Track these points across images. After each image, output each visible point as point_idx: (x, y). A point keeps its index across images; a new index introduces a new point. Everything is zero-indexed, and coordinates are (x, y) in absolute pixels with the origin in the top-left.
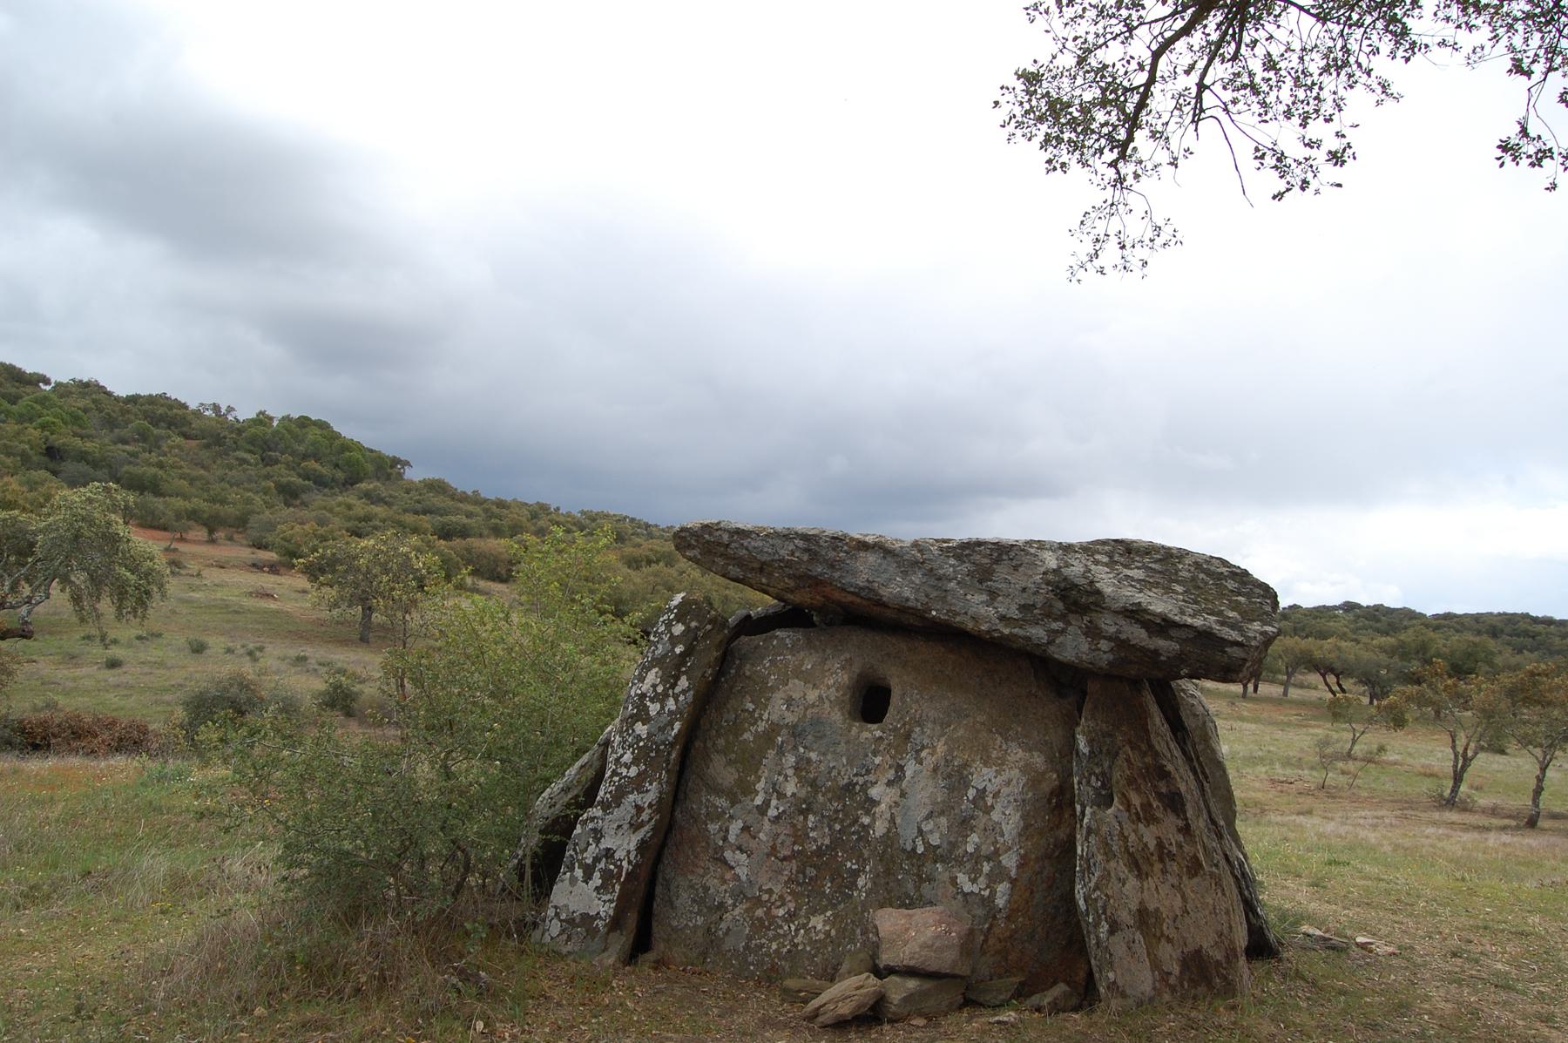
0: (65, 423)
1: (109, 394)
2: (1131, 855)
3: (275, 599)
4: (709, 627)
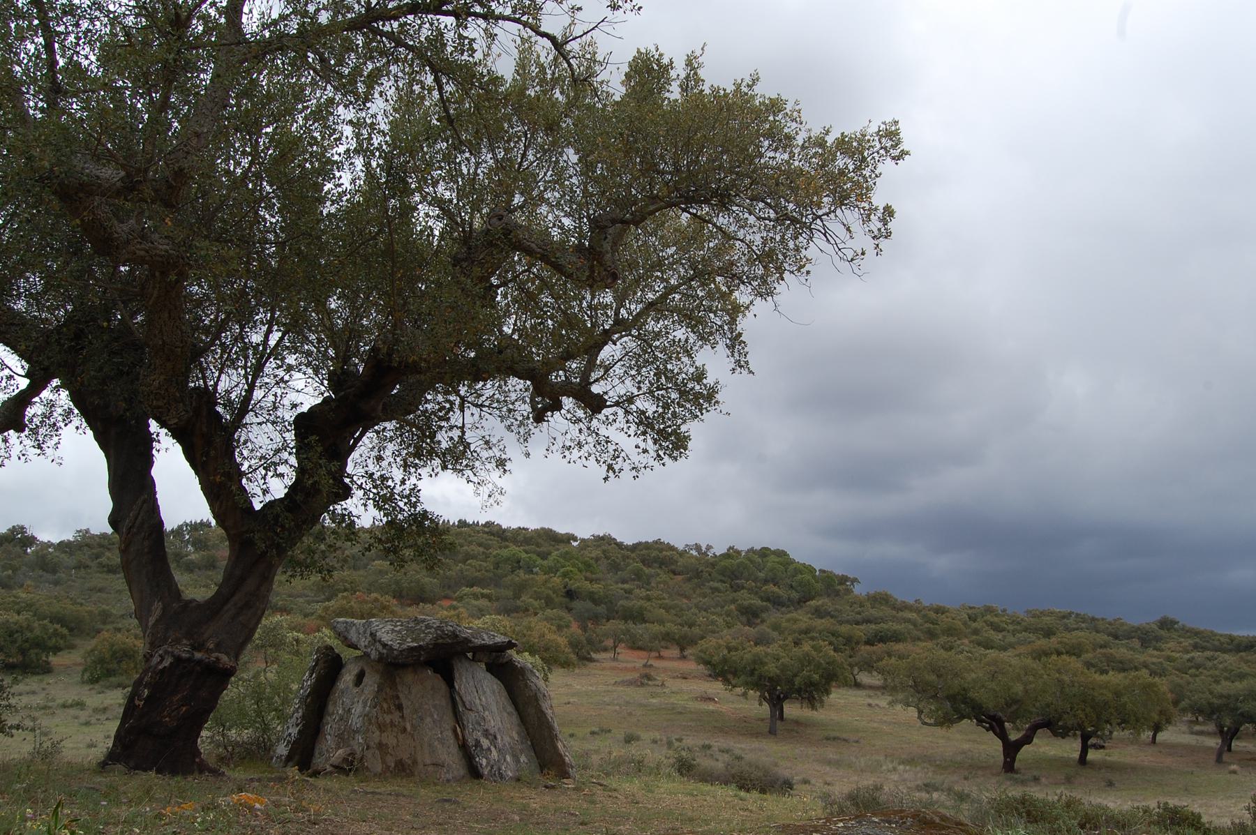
0: (580, 571)
1: (620, 545)
3: (716, 702)
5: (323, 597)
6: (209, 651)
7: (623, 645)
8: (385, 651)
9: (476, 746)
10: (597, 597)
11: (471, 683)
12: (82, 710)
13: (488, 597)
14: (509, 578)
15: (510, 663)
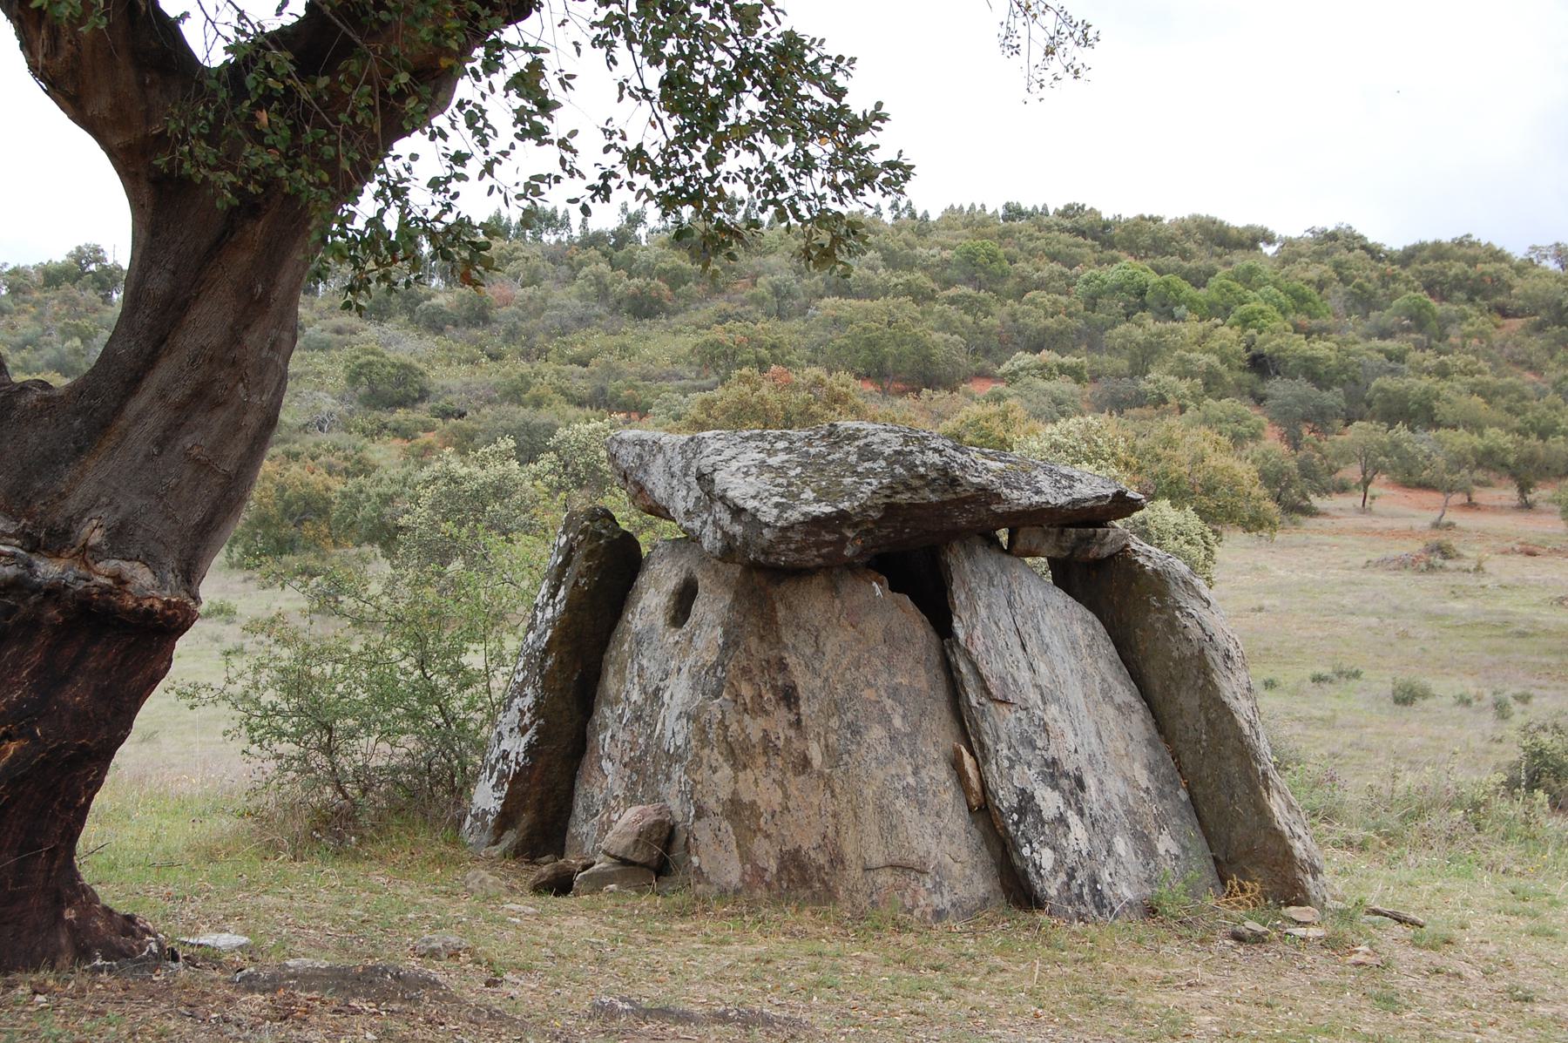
1: (1373, 252)
2: (729, 744)
4: (580, 537)
5: (715, 378)
6: (87, 554)
7: (1384, 477)
8: (737, 529)
10: (1321, 369)
11: (1006, 621)
12: (228, 622)
13: (1076, 374)
14: (1122, 328)
15: (1122, 563)
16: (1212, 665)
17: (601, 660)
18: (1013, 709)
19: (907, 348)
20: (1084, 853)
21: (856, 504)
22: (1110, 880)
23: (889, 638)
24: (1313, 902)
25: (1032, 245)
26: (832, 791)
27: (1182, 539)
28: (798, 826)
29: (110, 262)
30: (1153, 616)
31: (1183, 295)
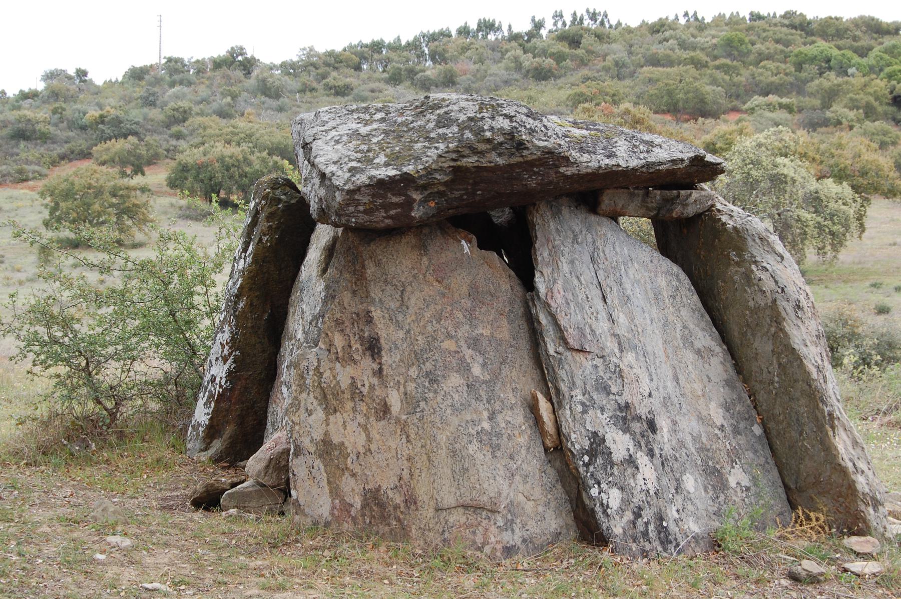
2: (322, 389)
4: (263, 202)
9: (592, 453)
11: (587, 275)
13: (789, 108)
14: (817, 82)
16: (783, 314)
17: (287, 303)
18: (590, 357)
19: (691, 95)
20: (652, 492)
21: (420, 167)
22: (677, 516)
23: (474, 292)
24: (873, 533)
25: (764, 35)
26: (408, 437)
27: (840, 202)
28: (379, 467)
29: (249, 56)
30: (733, 269)
31: (853, 61)
